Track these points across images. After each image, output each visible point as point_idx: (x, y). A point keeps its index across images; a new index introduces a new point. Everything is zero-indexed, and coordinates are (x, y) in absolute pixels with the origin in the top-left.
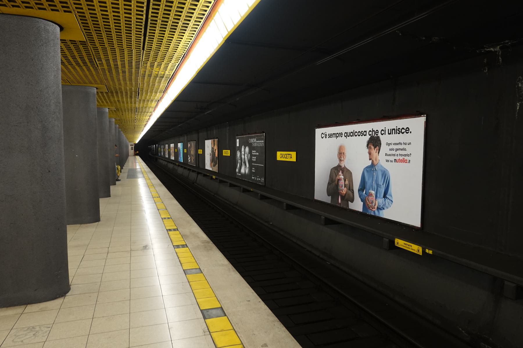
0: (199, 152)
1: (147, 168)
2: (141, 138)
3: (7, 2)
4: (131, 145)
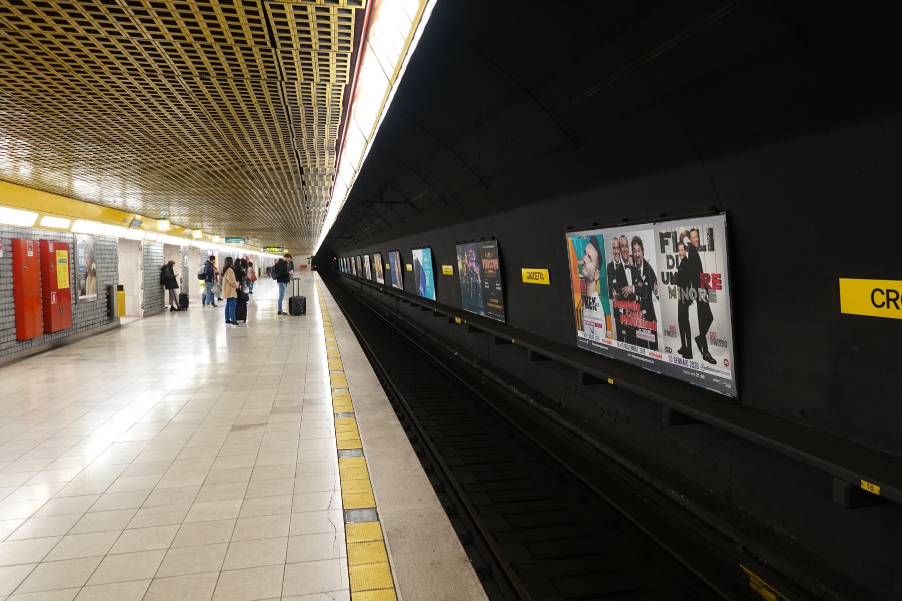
0: (444, 271)
1: (329, 296)
2: (330, 227)
3: (125, 4)
4: (308, 258)
